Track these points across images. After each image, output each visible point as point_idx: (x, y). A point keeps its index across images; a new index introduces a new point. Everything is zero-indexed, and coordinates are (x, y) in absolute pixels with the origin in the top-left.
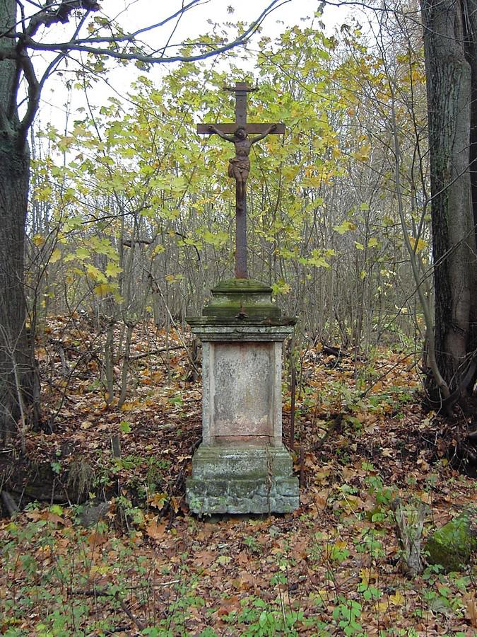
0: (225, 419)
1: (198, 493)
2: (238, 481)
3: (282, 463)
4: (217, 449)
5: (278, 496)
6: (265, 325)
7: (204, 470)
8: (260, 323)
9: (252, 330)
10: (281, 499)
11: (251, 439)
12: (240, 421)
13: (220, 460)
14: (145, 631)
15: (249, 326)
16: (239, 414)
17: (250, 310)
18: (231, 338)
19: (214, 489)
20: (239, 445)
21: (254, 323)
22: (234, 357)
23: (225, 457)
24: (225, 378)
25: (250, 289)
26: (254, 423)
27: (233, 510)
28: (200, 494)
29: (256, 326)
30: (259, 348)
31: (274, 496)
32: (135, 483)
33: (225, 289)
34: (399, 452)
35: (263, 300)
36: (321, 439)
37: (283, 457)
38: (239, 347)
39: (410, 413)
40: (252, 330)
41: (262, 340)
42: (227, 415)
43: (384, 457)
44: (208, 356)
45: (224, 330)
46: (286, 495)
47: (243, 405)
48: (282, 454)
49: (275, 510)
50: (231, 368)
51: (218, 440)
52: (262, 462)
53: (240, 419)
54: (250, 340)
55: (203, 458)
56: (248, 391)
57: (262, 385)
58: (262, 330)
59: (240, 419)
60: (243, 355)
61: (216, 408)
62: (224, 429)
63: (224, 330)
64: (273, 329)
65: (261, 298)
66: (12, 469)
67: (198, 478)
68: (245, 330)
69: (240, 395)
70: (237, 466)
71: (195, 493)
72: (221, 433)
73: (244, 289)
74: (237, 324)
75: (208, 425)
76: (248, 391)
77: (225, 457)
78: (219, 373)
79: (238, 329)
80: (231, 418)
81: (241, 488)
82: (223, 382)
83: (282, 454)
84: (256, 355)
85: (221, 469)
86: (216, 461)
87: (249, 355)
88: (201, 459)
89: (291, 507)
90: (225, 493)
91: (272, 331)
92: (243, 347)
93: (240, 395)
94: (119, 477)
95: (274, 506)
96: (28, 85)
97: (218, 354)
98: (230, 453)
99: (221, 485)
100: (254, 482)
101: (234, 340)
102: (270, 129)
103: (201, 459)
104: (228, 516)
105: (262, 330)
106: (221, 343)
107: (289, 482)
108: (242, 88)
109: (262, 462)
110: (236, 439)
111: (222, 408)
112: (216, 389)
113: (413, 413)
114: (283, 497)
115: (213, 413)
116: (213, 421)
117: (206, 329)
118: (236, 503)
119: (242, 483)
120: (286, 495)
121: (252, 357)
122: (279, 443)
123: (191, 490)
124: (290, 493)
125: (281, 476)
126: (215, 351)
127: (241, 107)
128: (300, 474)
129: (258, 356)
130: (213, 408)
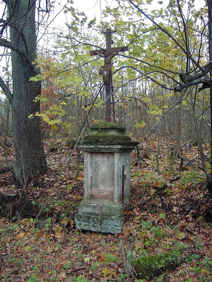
0: (95, 187)
1: (79, 220)
2: (95, 216)
3: (115, 210)
4: (89, 201)
5: (112, 226)
6: (108, 144)
7: (83, 210)
8: (106, 143)
9: (103, 147)
10: (113, 227)
11: (106, 197)
12: (102, 189)
13: (89, 206)
14: (204, 250)
15: (102, 145)
16: (101, 185)
17: (104, 137)
18: (95, 150)
19: (85, 219)
20: (101, 200)
21: (103, 143)
22: (99, 159)
23: (91, 205)
24: (96, 169)
25: (106, 127)
26: (107, 190)
27: (93, 229)
28: (80, 220)
29: (104, 145)
30: (110, 155)
31: (110, 226)
32: (59, 212)
33: (95, 128)
34: (181, 210)
35: (112, 132)
36: (137, 201)
37: (116, 207)
38: (101, 154)
39: (198, 189)
40: (103, 147)
41: (108, 151)
42: (97, 186)
43: (173, 212)
44: (87, 158)
45: (91, 147)
46: (114, 225)
47: (103, 181)
48: (116, 206)
49: (111, 232)
50: (98, 164)
51: (92, 197)
52: (106, 209)
53: (102, 187)
54: (103, 151)
55: (83, 204)
56: (105, 175)
57: (111, 172)
58: (107, 147)
59: (102, 187)
60: (103, 158)
61: (91, 182)
62: (94, 192)
63: (91, 147)
64: (111, 147)
65: (111, 131)
66: (19, 202)
67: (80, 213)
68: (100, 147)
69: (103, 176)
70: (96, 209)
71: (78, 220)
72: (94, 194)
73: (104, 127)
74: (96, 144)
75: (86, 190)
76: (105, 175)
77: (91, 205)
78: (93, 166)
79: (97, 146)
80: (98, 187)
81: (97, 220)
82: (95, 170)
83: (116, 206)
84: (109, 158)
85: (90, 210)
86: (87, 206)
87: (106, 158)
88: (82, 205)
89: (117, 231)
90: (90, 222)
91: (111, 148)
92: (103, 155)
93: (103, 176)
94: (55, 209)
95: (110, 230)
96: (10, 49)
97: (93, 157)
98: (94, 203)
99: (88, 217)
100: (102, 218)
101: (97, 151)
102: (120, 49)
103: (82, 205)
104: (90, 232)
105: (107, 147)
106: (93, 152)
107: (117, 220)
108: (109, 31)
109: (106, 209)
110: (100, 197)
111: (94, 182)
112: (92, 174)
113: (200, 189)
114: (114, 226)
115: (90, 184)
116: (89, 188)
117: (84, 146)
118: (94, 226)
119: (97, 217)
120: (114, 225)
121: (107, 159)
122: (116, 200)
123: (76, 218)
124: (117, 225)
125: (114, 216)
126: (91, 156)
127: (109, 41)
128: (126, 216)
129: (110, 159)
130: (90, 182)
